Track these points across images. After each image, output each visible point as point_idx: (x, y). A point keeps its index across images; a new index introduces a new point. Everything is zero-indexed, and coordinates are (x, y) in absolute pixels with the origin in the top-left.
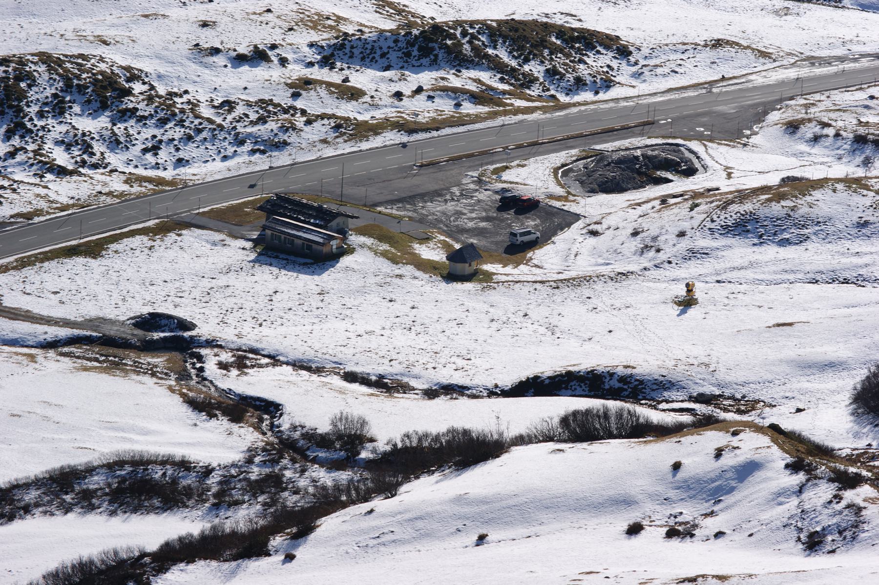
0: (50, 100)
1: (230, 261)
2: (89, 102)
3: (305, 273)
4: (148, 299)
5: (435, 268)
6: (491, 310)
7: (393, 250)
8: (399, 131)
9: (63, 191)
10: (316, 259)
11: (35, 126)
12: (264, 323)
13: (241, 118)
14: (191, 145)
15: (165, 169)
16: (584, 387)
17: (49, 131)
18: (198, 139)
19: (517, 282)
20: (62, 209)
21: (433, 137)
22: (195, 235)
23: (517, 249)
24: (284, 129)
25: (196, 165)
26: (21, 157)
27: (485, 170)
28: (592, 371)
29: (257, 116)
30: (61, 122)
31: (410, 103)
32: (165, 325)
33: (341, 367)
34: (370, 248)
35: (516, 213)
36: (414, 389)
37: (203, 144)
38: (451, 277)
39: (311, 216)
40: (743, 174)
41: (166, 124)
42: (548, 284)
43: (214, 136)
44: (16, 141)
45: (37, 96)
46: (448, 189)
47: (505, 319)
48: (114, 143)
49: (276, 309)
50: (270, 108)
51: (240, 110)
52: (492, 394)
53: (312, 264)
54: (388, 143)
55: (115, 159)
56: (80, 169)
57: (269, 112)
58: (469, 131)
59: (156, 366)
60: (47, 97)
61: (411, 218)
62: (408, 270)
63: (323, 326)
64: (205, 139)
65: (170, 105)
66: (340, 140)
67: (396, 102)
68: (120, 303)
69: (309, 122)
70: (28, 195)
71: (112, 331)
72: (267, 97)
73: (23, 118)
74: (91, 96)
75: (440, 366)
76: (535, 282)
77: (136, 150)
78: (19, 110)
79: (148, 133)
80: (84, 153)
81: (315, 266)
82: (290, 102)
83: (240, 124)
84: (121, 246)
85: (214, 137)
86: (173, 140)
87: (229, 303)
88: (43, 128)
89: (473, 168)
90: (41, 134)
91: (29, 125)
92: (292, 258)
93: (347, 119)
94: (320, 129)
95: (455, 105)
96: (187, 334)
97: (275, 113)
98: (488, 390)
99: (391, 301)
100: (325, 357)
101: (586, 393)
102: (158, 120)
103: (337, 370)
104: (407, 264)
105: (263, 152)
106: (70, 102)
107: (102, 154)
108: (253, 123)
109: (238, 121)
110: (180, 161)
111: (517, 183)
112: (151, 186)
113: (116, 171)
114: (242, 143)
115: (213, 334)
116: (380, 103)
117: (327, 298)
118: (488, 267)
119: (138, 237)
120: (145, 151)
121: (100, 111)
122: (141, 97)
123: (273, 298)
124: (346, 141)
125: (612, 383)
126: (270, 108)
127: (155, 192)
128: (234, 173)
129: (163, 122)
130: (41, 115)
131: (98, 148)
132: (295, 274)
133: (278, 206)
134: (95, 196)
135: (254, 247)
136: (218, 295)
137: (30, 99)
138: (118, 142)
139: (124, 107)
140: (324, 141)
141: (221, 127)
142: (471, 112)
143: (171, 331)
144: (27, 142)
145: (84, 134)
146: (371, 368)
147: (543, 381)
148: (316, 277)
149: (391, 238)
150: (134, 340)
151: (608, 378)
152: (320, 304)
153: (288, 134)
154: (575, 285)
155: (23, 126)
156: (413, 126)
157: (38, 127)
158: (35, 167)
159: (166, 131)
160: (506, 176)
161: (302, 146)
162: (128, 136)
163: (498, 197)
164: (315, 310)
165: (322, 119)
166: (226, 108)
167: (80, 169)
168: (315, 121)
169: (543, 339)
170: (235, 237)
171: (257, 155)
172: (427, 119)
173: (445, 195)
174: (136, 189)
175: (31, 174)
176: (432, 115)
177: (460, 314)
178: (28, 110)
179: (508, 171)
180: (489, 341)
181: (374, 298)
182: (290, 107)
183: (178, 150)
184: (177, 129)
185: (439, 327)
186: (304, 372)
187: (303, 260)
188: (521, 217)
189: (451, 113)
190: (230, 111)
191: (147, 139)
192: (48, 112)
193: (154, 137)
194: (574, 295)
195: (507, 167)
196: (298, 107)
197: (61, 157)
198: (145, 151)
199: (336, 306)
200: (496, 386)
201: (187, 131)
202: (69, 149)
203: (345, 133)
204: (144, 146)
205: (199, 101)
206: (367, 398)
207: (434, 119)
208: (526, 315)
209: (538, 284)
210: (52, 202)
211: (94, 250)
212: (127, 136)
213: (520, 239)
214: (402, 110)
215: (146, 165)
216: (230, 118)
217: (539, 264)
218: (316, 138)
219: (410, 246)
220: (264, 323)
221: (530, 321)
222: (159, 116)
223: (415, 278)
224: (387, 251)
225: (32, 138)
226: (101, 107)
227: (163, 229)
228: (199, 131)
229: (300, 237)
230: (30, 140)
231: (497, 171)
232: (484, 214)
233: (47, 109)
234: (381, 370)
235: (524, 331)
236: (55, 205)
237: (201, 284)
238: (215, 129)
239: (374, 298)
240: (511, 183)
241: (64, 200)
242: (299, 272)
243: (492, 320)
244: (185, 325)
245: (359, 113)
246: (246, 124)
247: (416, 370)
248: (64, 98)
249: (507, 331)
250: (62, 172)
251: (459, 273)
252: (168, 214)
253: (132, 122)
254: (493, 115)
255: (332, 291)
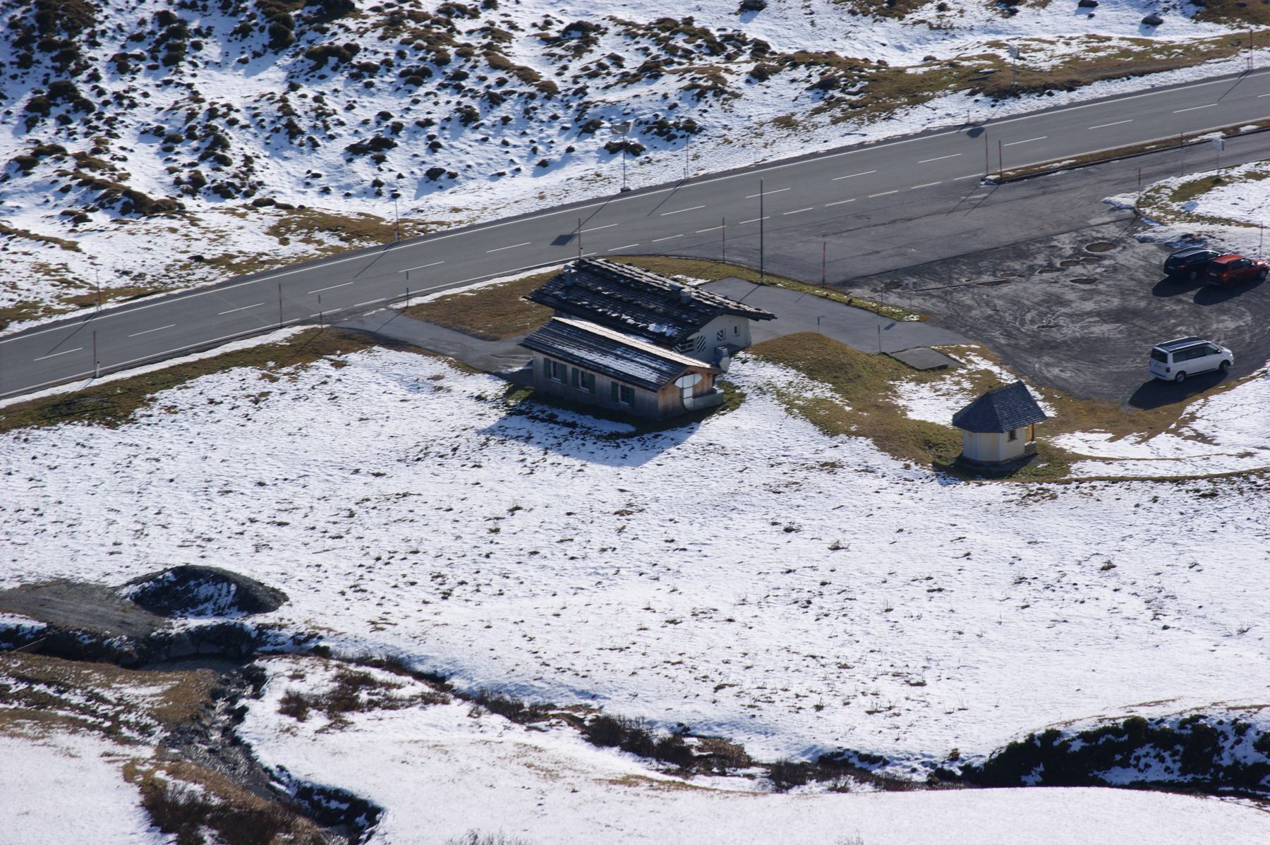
0: (149, 28)
1: (433, 430)
2: (244, 31)
3: (605, 461)
4: (200, 527)
5: (929, 444)
6: (1028, 553)
7: (838, 399)
8: (972, 94)
9: (113, 253)
10: (633, 420)
11: (101, 93)
12: (458, 591)
13: (601, 66)
14: (471, 135)
15: (395, 196)
16: (1169, 762)
17: (133, 105)
18: (487, 120)
19: (1114, 480)
20: (82, 303)
21: (1057, 107)
22: (378, 364)
23: (1162, 396)
24: (697, 93)
25: (472, 185)
26: (44, 171)
27: (1157, 191)
28: (1195, 719)
29: (641, 60)
30: (168, 83)
31: (1032, 22)
32: (207, 599)
33: (594, 704)
34: (780, 395)
35: (1200, 300)
36: (750, 763)
37: (498, 134)
38: (965, 469)
39: (652, 316)
40: (732, 270)
41: (419, 83)
42: (1191, 486)
43: (527, 111)
44: (46, 132)
45: (119, 20)
46: (1049, 238)
47: (1052, 576)
48: (286, 131)
49: (499, 554)
50: (680, 41)
51: (606, 46)
52: (940, 778)
53: (629, 436)
54: (937, 124)
55: (280, 177)
56: (187, 201)
57: (673, 50)
58: (1154, 89)
59: (130, 708)
60: (142, 22)
61: (926, 316)
62: (859, 449)
63: (601, 597)
64: (505, 120)
65: (439, 37)
66: (824, 118)
67: (999, 19)
68: (127, 541)
69: (759, 75)
70: (18, 267)
71: (73, 618)
72: (678, 15)
73: (75, 73)
74: (252, 17)
75: (838, 702)
76: (1161, 480)
77: (332, 152)
78: (68, 54)
79: (369, 108)
80: (202, 159)
81: (634, 442)
82: (733, 25)
83: (599, 82)
84: (188, 393)
85: (528, 114)
86: (429, 123)
87: (388, 540)
88: (119, 97)
89: (1124, 185)
90: (109, 112)
91: (85, 91)
92: (588, 421)
93: (851, 65)
94: (785, 91)
95: (1145, 21)
96: (252, 622)
97: (687, 54)
98: (933, 765)
99: (788, 530)
100: (560, 678)
101: (1174, 777)
102: (402, 75)
103: (579, 715)
104: (857, 434)
105: (634, 151)
106: (198, 32)
107: (248, 160)
108: (628, 79)
109: (593, 75)
110: (434, 174)
111: (1228, 222)
112: (331, 240)
113: (270, 202)
114: (589, 128)
115: (321, 621)
116: (957, 22)
117: (635, 524)
118: (1070, 442)
119: (236, 370)
120: (355, 151)
121: (269, 55)
122: (374, 18)
123: (502, 525)
124: (835, 121)
125: (1240, 751)
126: (680, 41)
127: (338, 253)
128: (550, 202)
129: (415, 78)
130: (121, 65)
131: (239, 144)
132: (577, 464)
133: (593, 289)
134: (183, 267)
135: (508, 394)
136: (374, 518)
137: (99, 28)
138: (293, 131)
139: (326, 43)
140: (786, 122)
141: (549, 90)
142: (1177, 39)
143: (219, 614)
144: (71, 134)
145: (212, 113)
146: (656, 710)
147: (1066, 745)
148: (626, 471)
149: (842, 367)
150: (120, 640)
151: (1232, 739)
152: (613, 540)
153: (702, 106)
154: (1259, 488)
155: (69, 92)
156: (1008, 81)
157: (107, 97)
158: (71, 196)
159: (416, 102)
160: (1207, 204)
161: (731, 136)
162: (321, 114)
163: (1164, 257)
164: (594, 554)
165: (795, 66)
166: (573, 42)
167: (187, 201)
168: (776, 71)
169: (1125, 629)
170: (468, 367)
171: (619, 159)
172: (1056, 62)
173: (1034, 255)
174: (296, 247)
175: (57, 212)
176: (1074, 49)
177: (941, 564)
178: (92, 53)
179: (1216, 192)
180: (991, 635)
181: (750, 524)
182: (728, 38)
183: (434, 147)
184: (443, 96)
185: (881, 597)
186: (498, 720)
187: (608, 427)
188: (1206, 309)
189: (1124, 44)
190: (578, 51)
191: (365, 122)
192: (140, 58)
193: (385, 116)
194: (1248, 512)
195: (1217, 181)
196: (750, 36)
197: (145, 172)
198: (355, 151)
199: (652, 544)
200: (954, 756)
201: (466, 101)
202: (169, 150)
203: (839, 101)
204: (356, 140)
205: (513, 26)
206: (600, 791)
207: (1074, 61)
208: (1109, 567)
209: (1167, 485)
210: (69, 284)
211: (112, 408)
212: (318, 116)
213: (1175, 367)
214: (1002, 38)
215: (349, 186)
216: (575, 67)
217: (1208, 432)
218: (768, 114)
219: (890, 388)
220: (458, 591)
221: (1112, 583)
222: (405, 65)
223: (868, 470)
224: (818, 402)
225: (87, 122)
226: (271, 45)
227: (302, 352)
228: (494, 101)
229: (604, 370)
230: (81, 129)
231: (1188, 192)
232: (1116, 302)
233: (137, 51)
234: (684, 713)
235: (1088, 608)
236: (73, 292)
237: (345, 490)
238: (532, 96)
239: (750, 524)
240: (1213, 220)
241: (105, 278)
242: (591, 457)
243: (1021, 580)
244: (255, 597)
245: (901, 48)
246: (611, 80)
247: (768, 714)
248: (184, 23)
249: (1045, 610)
250: (137, 205)
251: (983, 456)
252: (316, 314)
253: (338, 81)
254: (1226, 47)
255: (654, 506)
